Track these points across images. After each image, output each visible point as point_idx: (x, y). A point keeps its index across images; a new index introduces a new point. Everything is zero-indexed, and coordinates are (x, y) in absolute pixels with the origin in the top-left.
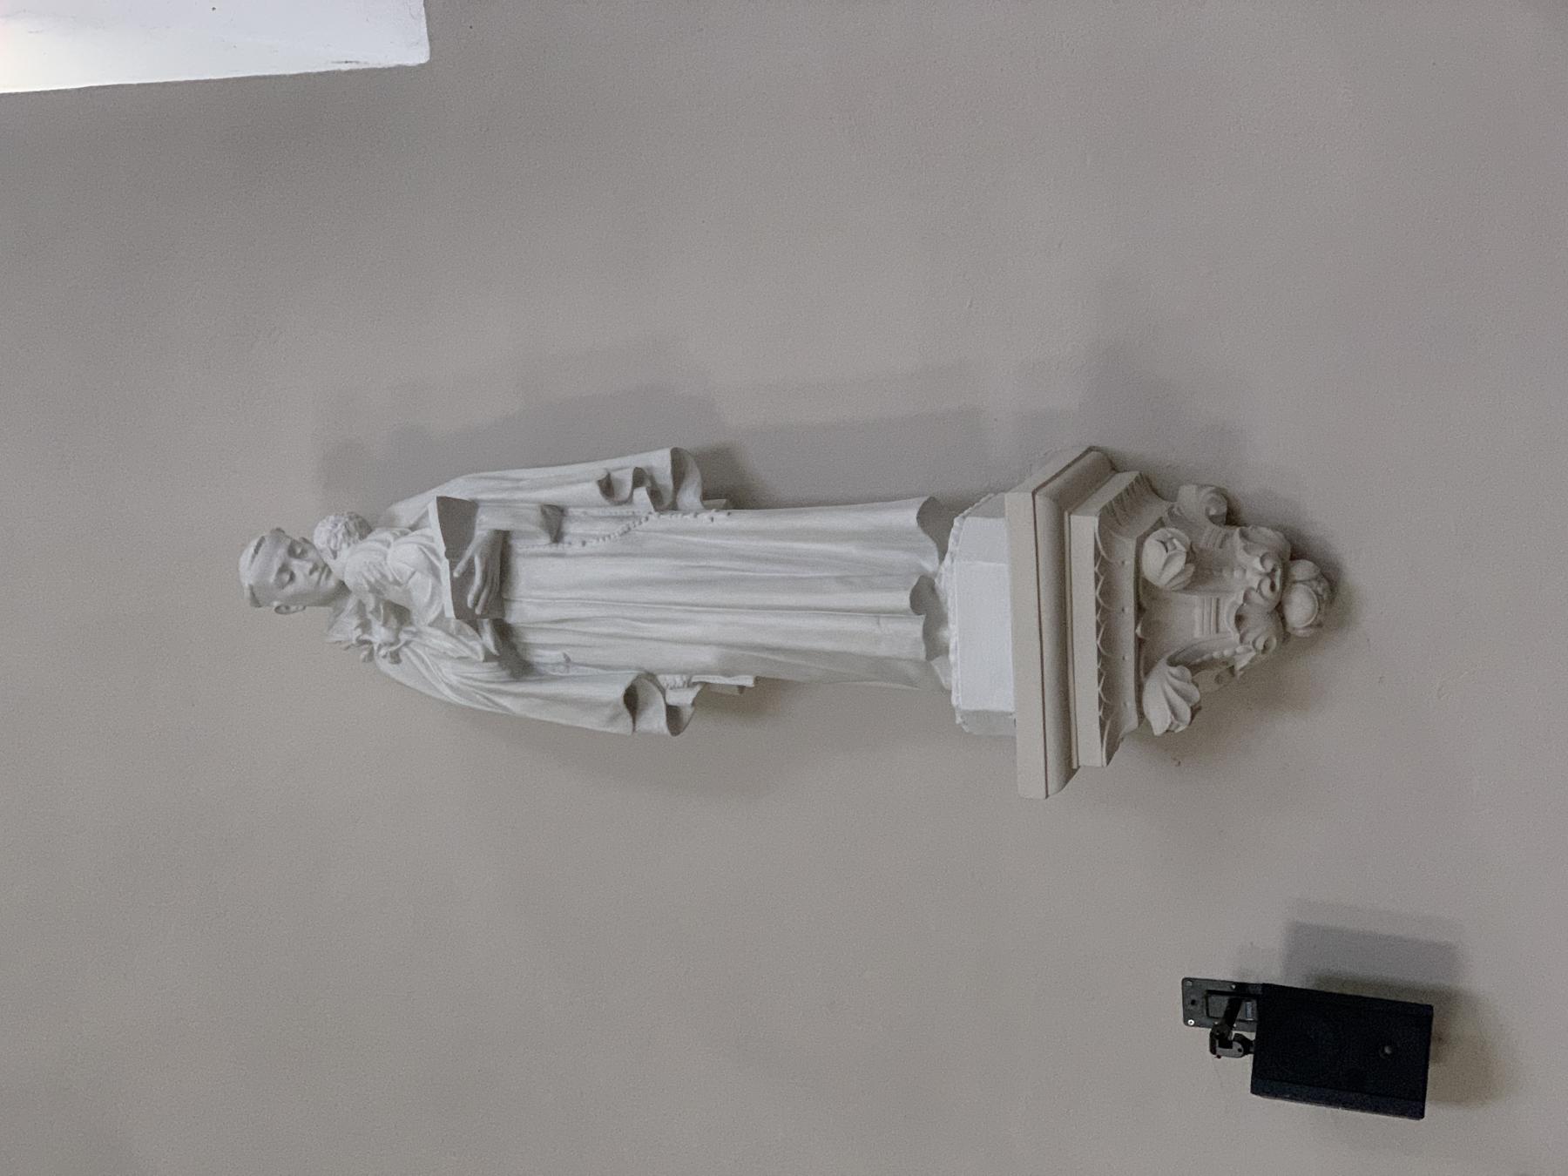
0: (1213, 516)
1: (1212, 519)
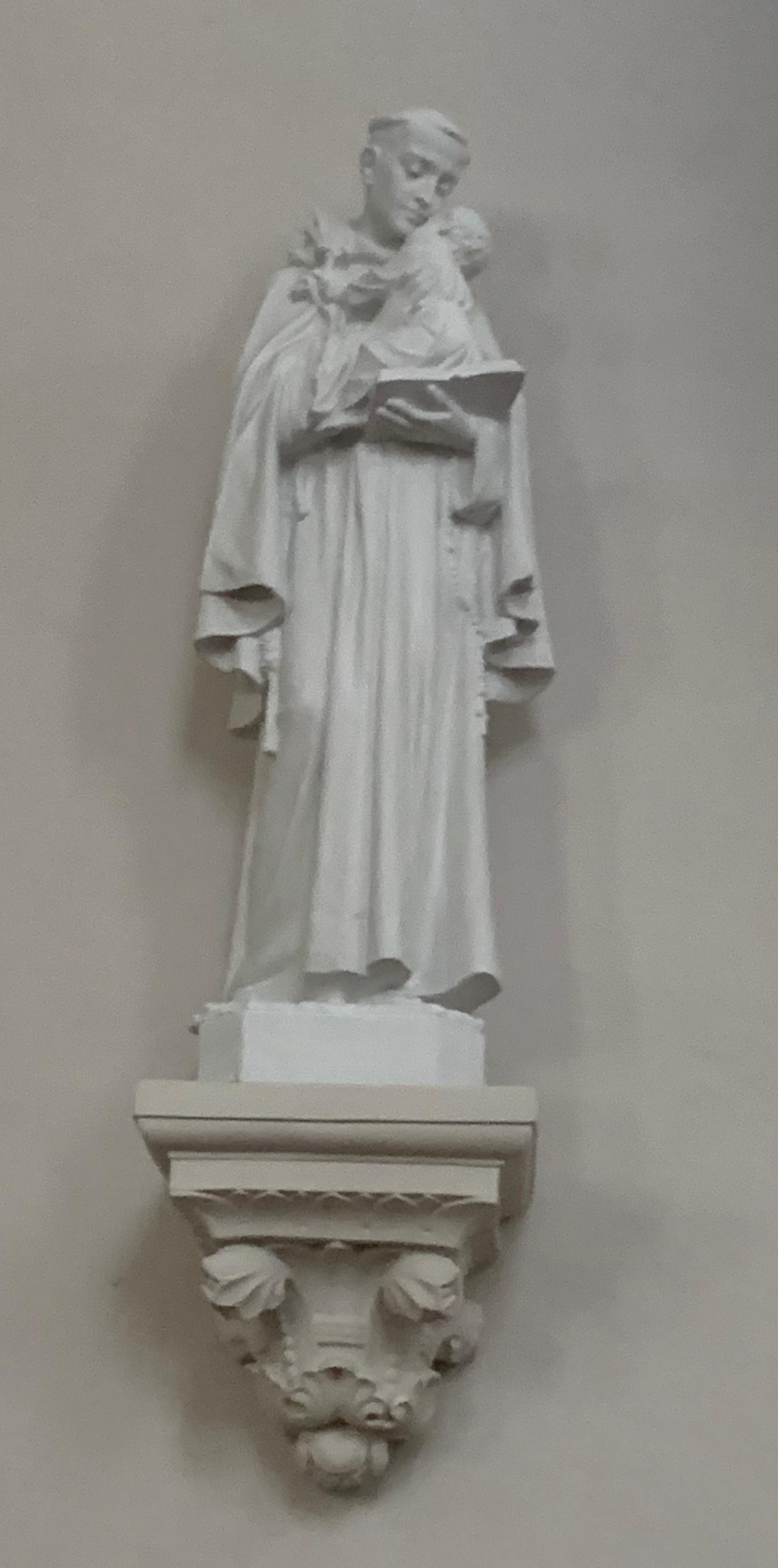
0: (450, 1347)
1: (446, 1345)
